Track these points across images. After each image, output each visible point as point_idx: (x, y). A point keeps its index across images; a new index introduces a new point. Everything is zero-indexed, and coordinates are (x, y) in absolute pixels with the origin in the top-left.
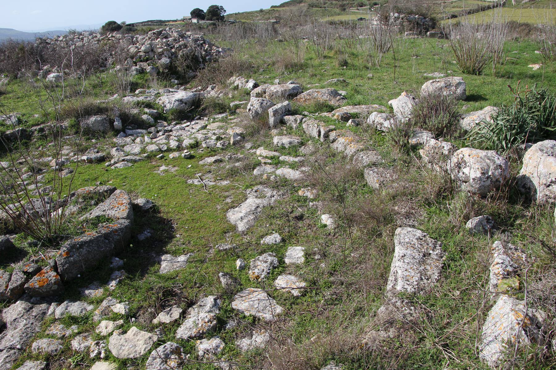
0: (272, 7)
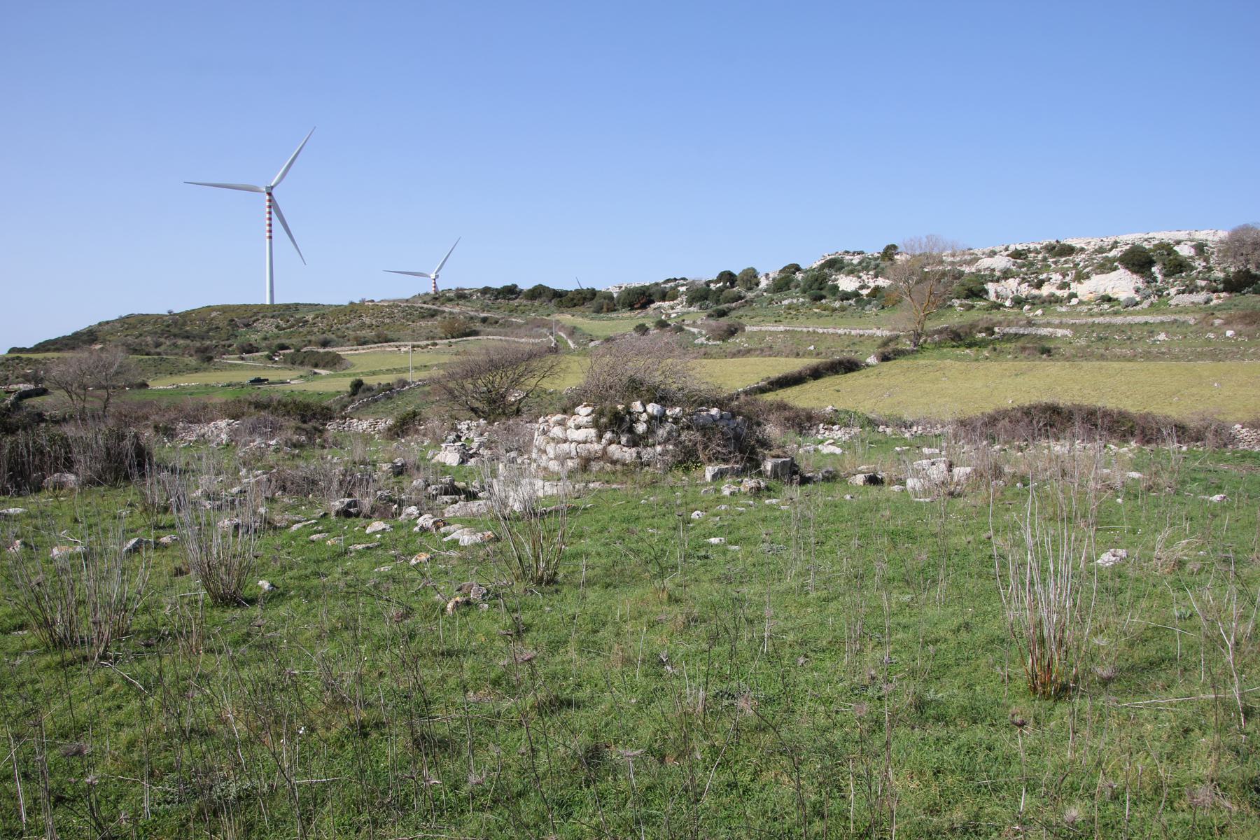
0: (12, 350)
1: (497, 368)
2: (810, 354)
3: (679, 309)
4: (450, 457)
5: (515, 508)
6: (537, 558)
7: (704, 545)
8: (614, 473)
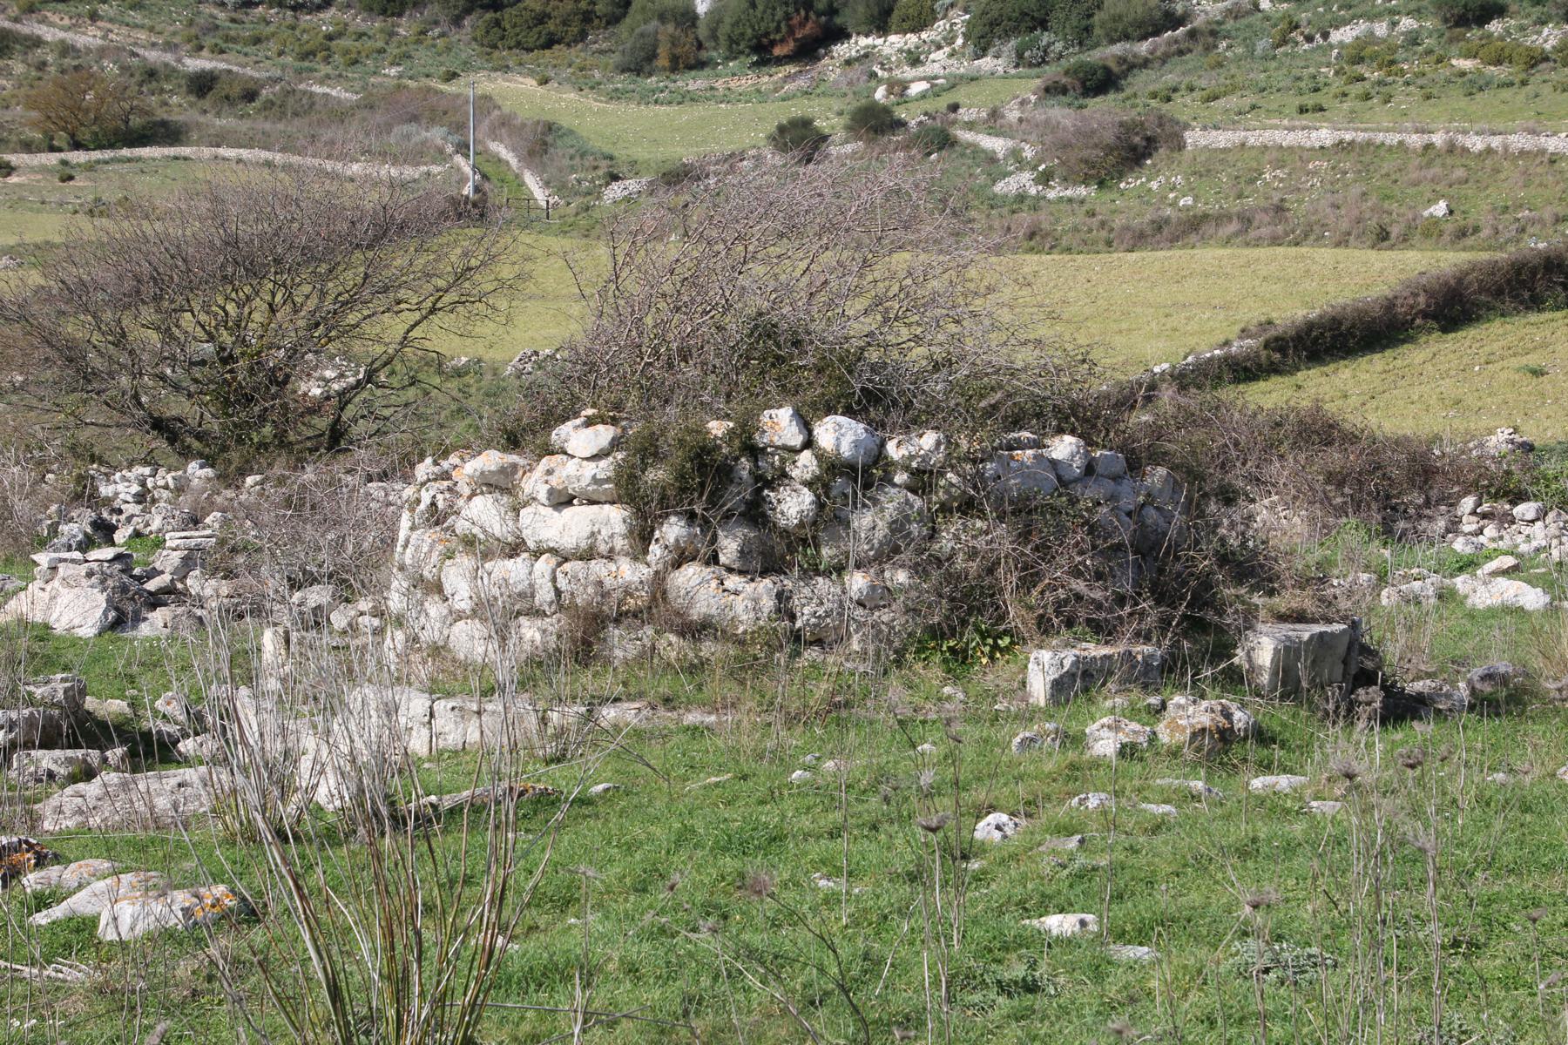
1: (255, 272)
2: (1432, 231)
3: (938, 62)
4: (69, 603)
5: (321, 796)
6: (400, 985)
7: (1022, 942)
8: (695, 669)
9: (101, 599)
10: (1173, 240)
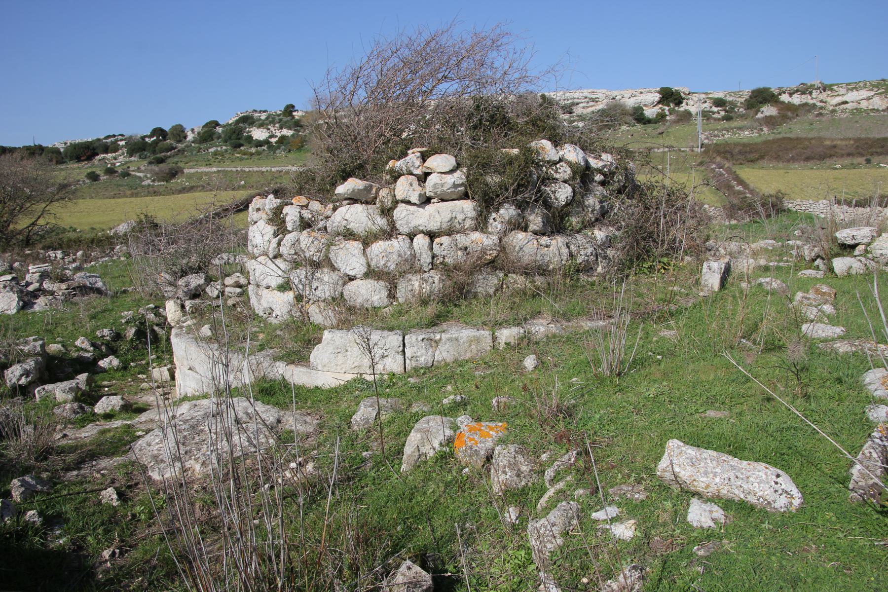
3: (121, 158)
9: (15, 297)
10: (188, 192)
